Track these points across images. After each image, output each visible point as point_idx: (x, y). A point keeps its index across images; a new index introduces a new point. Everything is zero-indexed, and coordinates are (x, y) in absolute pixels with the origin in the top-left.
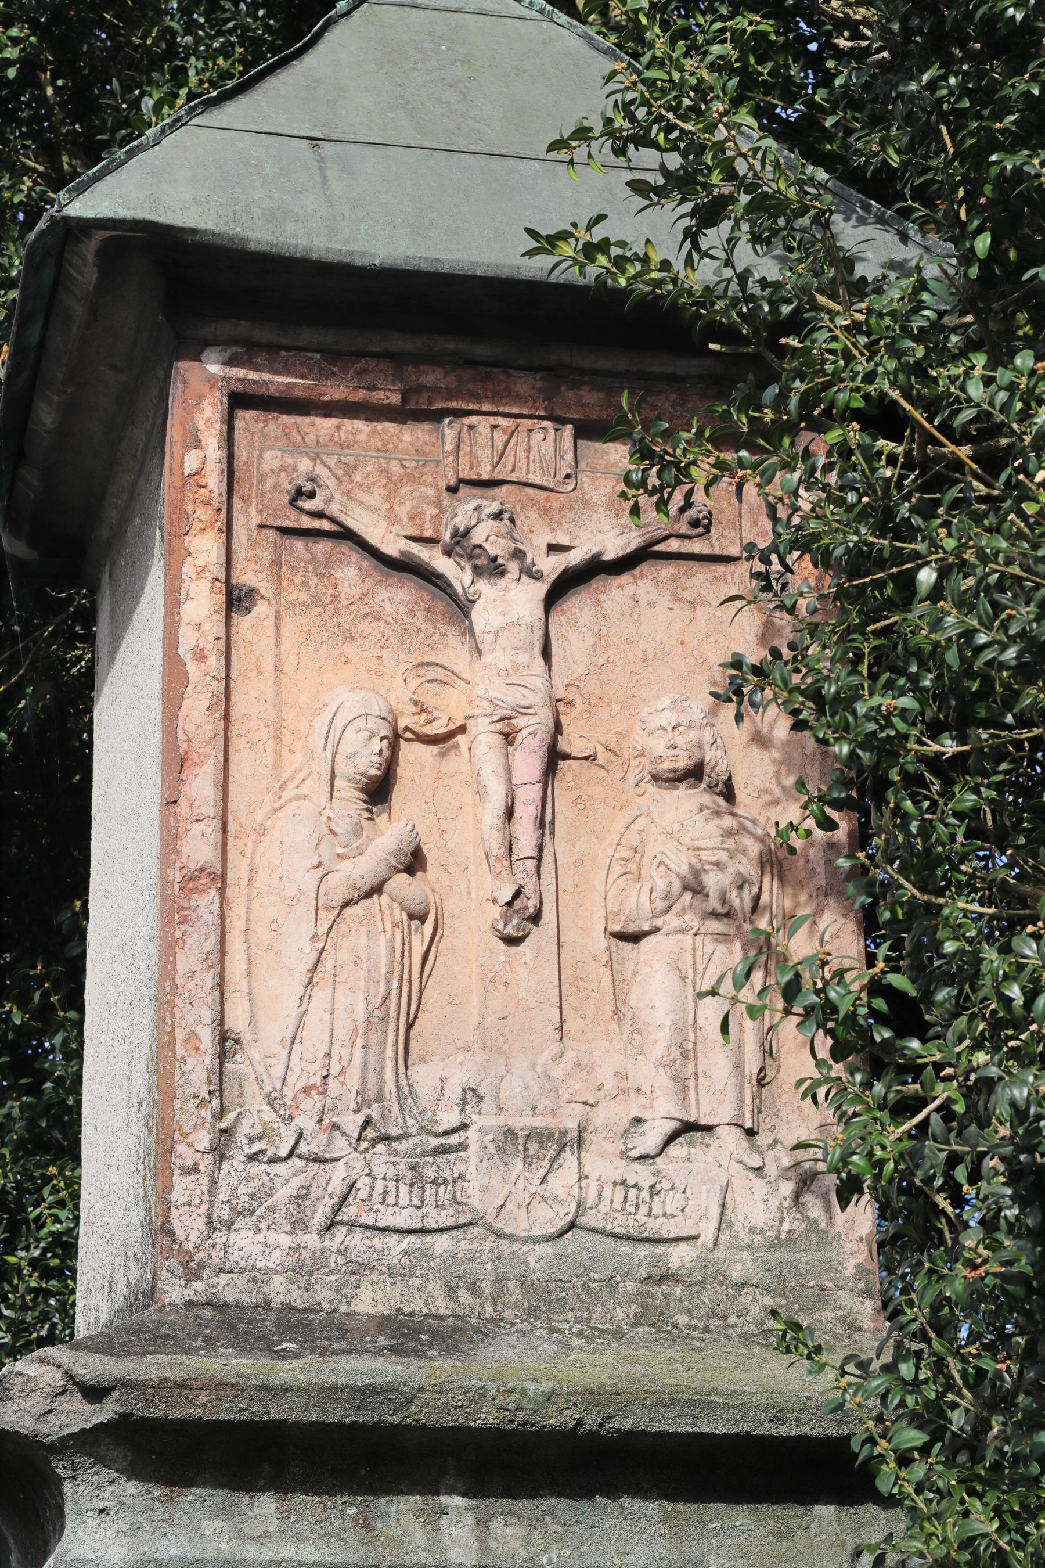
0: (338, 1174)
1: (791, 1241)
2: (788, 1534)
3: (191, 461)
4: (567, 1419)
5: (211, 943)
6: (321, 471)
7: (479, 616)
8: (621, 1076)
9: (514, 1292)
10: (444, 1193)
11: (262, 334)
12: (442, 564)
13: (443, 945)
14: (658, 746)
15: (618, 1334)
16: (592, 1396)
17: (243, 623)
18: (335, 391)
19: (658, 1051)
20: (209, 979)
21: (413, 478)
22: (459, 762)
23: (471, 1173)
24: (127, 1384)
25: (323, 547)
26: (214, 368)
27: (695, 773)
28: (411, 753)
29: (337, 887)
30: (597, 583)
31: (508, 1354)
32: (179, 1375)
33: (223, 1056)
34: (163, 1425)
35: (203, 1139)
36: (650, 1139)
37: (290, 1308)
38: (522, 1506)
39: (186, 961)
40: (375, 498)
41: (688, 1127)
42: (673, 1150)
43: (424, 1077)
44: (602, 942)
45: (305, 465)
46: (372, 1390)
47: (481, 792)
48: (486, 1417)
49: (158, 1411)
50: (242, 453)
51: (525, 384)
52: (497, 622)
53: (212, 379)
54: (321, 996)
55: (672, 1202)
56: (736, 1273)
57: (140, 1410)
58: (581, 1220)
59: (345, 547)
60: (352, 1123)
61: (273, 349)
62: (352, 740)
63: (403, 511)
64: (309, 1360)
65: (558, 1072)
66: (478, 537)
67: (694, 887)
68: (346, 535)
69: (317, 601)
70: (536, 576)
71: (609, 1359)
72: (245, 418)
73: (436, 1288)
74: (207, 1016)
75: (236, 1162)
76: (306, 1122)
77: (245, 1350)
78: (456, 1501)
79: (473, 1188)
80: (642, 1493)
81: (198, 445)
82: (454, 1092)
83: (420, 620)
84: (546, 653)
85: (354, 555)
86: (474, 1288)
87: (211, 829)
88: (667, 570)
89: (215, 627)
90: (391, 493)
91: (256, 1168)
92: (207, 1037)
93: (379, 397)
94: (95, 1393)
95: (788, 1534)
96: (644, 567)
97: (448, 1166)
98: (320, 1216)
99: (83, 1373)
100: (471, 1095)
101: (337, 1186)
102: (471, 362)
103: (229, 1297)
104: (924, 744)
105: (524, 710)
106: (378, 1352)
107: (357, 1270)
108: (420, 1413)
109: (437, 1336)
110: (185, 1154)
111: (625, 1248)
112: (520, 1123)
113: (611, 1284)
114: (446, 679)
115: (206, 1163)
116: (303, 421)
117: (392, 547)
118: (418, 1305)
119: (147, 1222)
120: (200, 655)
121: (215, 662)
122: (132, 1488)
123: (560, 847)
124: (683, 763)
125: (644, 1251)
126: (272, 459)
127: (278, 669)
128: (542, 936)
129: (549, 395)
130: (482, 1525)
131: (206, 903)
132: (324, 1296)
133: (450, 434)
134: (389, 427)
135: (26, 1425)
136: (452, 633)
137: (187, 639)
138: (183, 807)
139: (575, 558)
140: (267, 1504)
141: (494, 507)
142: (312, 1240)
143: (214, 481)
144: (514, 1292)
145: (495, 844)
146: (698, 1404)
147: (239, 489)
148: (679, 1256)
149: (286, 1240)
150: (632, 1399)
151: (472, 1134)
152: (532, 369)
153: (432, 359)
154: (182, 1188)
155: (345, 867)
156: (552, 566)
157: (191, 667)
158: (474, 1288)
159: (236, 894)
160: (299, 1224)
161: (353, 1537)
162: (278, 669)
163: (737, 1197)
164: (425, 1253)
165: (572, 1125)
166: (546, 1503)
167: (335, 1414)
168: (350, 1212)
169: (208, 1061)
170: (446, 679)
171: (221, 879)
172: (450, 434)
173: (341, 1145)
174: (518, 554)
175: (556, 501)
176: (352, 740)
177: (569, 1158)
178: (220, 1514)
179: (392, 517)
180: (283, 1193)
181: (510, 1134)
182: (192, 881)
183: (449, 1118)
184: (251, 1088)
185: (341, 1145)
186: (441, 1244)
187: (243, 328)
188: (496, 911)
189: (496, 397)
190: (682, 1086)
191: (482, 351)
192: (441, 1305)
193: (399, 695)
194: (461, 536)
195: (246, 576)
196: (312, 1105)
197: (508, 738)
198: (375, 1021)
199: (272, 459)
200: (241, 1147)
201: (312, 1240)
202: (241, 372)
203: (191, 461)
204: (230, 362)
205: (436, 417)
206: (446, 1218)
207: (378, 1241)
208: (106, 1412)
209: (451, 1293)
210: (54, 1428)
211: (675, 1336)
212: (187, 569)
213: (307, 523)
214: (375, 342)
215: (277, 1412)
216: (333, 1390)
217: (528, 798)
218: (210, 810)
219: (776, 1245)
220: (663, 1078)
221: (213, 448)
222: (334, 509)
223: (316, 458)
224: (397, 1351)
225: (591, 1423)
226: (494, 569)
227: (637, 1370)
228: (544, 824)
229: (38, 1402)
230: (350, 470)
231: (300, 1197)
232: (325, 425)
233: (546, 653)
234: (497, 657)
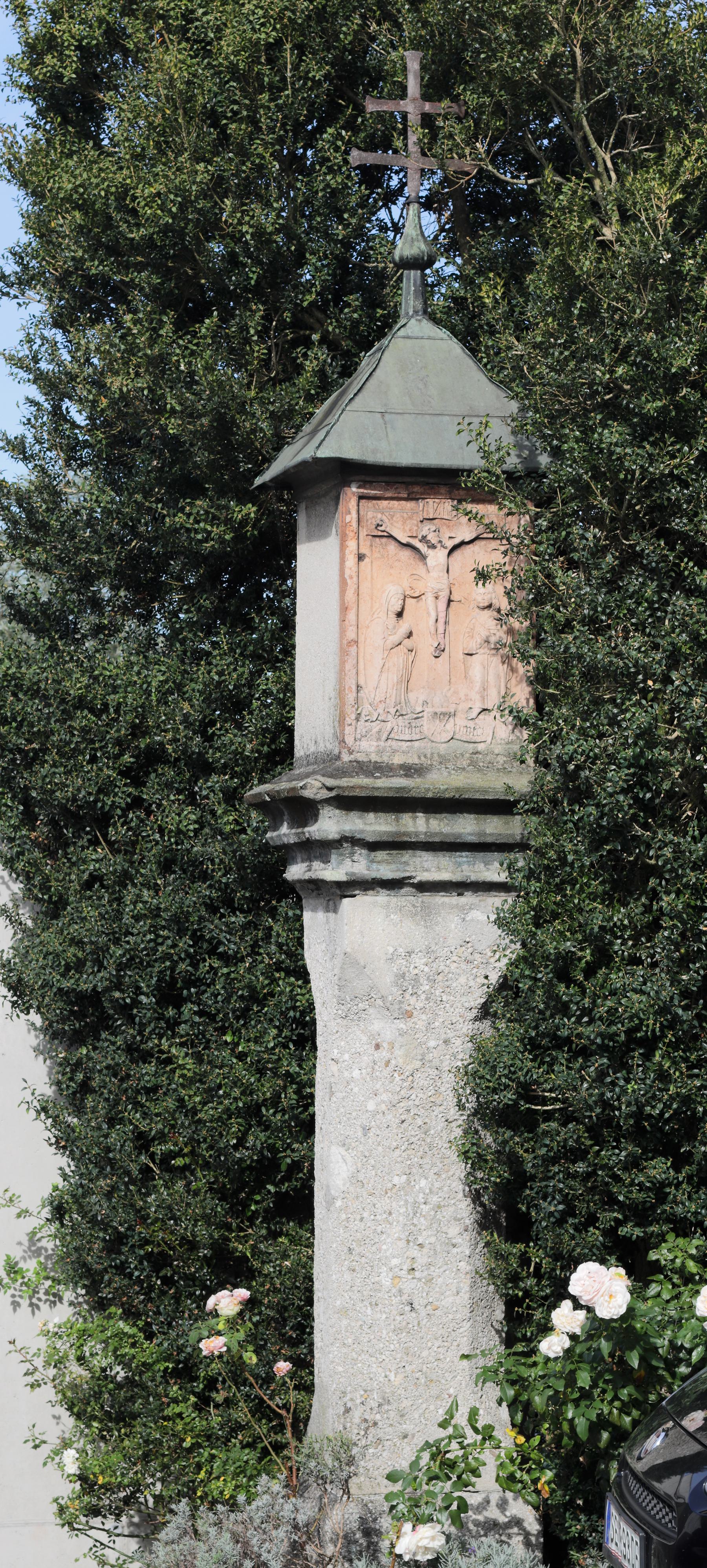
0: (389, 726)
1: (512, 742)
2: (508, 823)
3: (348, 518)
4: (451, 795)
5: (355, 662)
6: (384, 518)
7: (428, 560)
8: (466, 695)
9: (436, 757)
10: (417, 730)
11: (368, 479)
12: (419, 545)
13: (417, 658)
14: (479, 599)
15: (464, 769)
16: (458, 789)
17: (362, 564)
18: (389, 494)
19: (477, 689)
20: (354, 671)
21: (410, 518)
22: (422, 603)
23: (425, 723)
24: (339, 787)
25: (384, 540)
26: (354, 489)
27: (489, 606)
28: (409, 601)
29: (389, 644)
30: (463, 547)
31: (435, 776)
32: (351, 784)
33: (358, 692)
34: (347, 797)
35: (353, 716)
36: (474, 715)
37: (376, 762)
38: (438, 816)
39: (348, 666)
40: (399, 525)
41: (484, 710)
42: (481, 716)
43: (412, 696)
44: (461, 656)
45: (379, 516)
46: (401, 788)
47: (428, 614)
48: (430, 795)
49: (346, 794)
50: (361, 513)
51: (443, 490)
52: (434, 563)
53: (354, 493)
54: (384, 675)
55: (479, 731)
56: (496, 752)
57: (341, 793)
58: (456, 737)
59: (390, 540)
60: (393, 711)
61: (371, 482)
62: (393, 600)
63: (407, 528)
64: (384, 779)
65: (449, 695)
66: (429, 538)
67: (487, 641)
68: (390, 536)
69: (383, 556)
70: (446, 548)
71: (461, 778)
72: (363, 502)
73: (415, 757)
74: (354, 682)
75: (362, 722)
76: (380, 710)
77: (367, 776)
78: (421, 814)
79: (425, 728)
80: (469, 812)
81: (350, 513)
82: (420, 702)
83: (412, 561)
84: (448, 571)
85: (393, 542)
86: (425, 756)
87: (355, 628)
88: (483, 543)
89: (355, 569)
90: (404, 523)
91: (368, 724)
92: (354, 688)
93: (401, 495)
94: (330, 789)
95: (508, 823)
96: (477, 542)
97: (418, 722)
98: (384, 737)
99: (328, 784)
100: (425, 703)
101: (389, 729)
102: (428, 484)
103: (360, 759)
104: (633, 130)
105: (440, 590)
106: (401, 776)
107: (394, 752)
108: (413, 794)
109: (416, 770)
110: (348, 720)
111: (466, 745)
112: (439, 710)
113: (462, 755)
114: (419, 578)
115: (354, 723)
116: (379, 502)
117: (404, 541)
118: (410, 761)
119: (335, 734)
120: (351, 577)
121: (355, 579)
122: (337, 811)
123: (450, 628)
124: (486, 604)
125: (472, 745)
126: (370, 514)
127: (372, 578)
128: (445, 655)
129: (450, 493)
130: (427, 820)
131: (353, 650)
132: (385, 759)
133: (421, 505)
134: (403, 503)
135: (312, 796)
136: (421, 564)
137: (347, 573)
138: (347, 622)
139: (457, 541)
140: (371, 815)
141: (434, 528)
142: (382, 744)
143: (354, 524)
144: (436, 757)
145: (433, 630)
146: (486, 792)
147: (362, 524)
148: (481, 747)
149: (375, 744)
150: (468, 790)
151: (425, 714)
152: (445, 485)
153: (417, 484)
154: (348, 730)
155: (391, 638)
156: (450, 544)
157: (349, 581)
158: (425, 756)
159: (361, 645)
160: (379, 739)
161: (394, 824)
162: (372, 578)
163: (497, 730)
164: (412, 747)
165: (452, 711)
166: (444, 815)
167: (391, 794)
168: (392, 736)
169: (354, 695)
170: (419, 578)
171: (357, 642)
172: (421, 505)
173: (390, 717)
174: (440, 542)
175: (451, 523)
176: (393, 600)
177: (451, 719)
178: (360, 818)
179: (404, 530)
180: (375, 730)
181: (436, 713)
182: (349, 644)
183: (419, 709)
184: (365, 701)
185: (390, 717)
186: (416, 744)
187: (363, 477)
188: (433, 649)
189: (435, 494)
190: (483, 699)
191: (431, 481)
192: (416, 761)
193: (406, 584)
194: (424, 537)
195: (362, 551)
196: (382, 706)
197: (437, 598)
198: (399, 682)
199: (370, 514)
200: (363, 718)
201: (382, 744)
202: (361, 490)
203: (348, 518)
204: (359, 487)
205: (417, 499)
206: (418, 737)
207: (400, 743)
208: (333, 794)
209: (419, 757)
210: (319, 797)
211: (480, 770)
212: (347, 551)
213: (380, 534)
214: (400, 479)
215: (376, 794)
216: (391, 788)
217: (442, 615)
218: (354, 623)
219: (508, 743)
220: (478, 697)
221: (354, 514)
222: (388, 530)
223: (383, 513)
224: (406, 775)
225: (457, 796)
226: (433, 547)
227: (469, 781)
228: (446, 623)
229: (315, 790)
230: (392, 516)
231: (379, 732)
232: (385, 503)
233: (448, 571)
234: (434, 574)
